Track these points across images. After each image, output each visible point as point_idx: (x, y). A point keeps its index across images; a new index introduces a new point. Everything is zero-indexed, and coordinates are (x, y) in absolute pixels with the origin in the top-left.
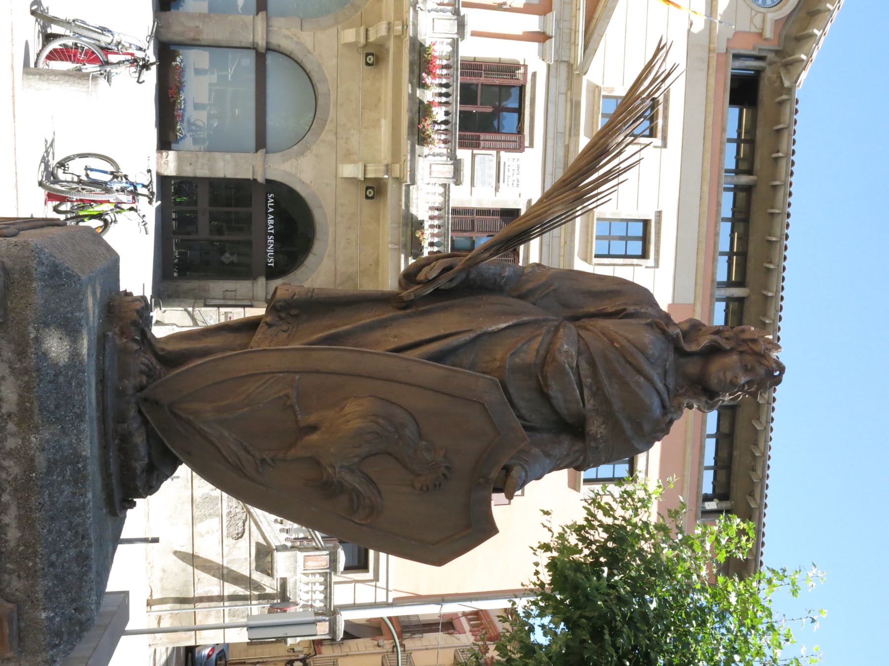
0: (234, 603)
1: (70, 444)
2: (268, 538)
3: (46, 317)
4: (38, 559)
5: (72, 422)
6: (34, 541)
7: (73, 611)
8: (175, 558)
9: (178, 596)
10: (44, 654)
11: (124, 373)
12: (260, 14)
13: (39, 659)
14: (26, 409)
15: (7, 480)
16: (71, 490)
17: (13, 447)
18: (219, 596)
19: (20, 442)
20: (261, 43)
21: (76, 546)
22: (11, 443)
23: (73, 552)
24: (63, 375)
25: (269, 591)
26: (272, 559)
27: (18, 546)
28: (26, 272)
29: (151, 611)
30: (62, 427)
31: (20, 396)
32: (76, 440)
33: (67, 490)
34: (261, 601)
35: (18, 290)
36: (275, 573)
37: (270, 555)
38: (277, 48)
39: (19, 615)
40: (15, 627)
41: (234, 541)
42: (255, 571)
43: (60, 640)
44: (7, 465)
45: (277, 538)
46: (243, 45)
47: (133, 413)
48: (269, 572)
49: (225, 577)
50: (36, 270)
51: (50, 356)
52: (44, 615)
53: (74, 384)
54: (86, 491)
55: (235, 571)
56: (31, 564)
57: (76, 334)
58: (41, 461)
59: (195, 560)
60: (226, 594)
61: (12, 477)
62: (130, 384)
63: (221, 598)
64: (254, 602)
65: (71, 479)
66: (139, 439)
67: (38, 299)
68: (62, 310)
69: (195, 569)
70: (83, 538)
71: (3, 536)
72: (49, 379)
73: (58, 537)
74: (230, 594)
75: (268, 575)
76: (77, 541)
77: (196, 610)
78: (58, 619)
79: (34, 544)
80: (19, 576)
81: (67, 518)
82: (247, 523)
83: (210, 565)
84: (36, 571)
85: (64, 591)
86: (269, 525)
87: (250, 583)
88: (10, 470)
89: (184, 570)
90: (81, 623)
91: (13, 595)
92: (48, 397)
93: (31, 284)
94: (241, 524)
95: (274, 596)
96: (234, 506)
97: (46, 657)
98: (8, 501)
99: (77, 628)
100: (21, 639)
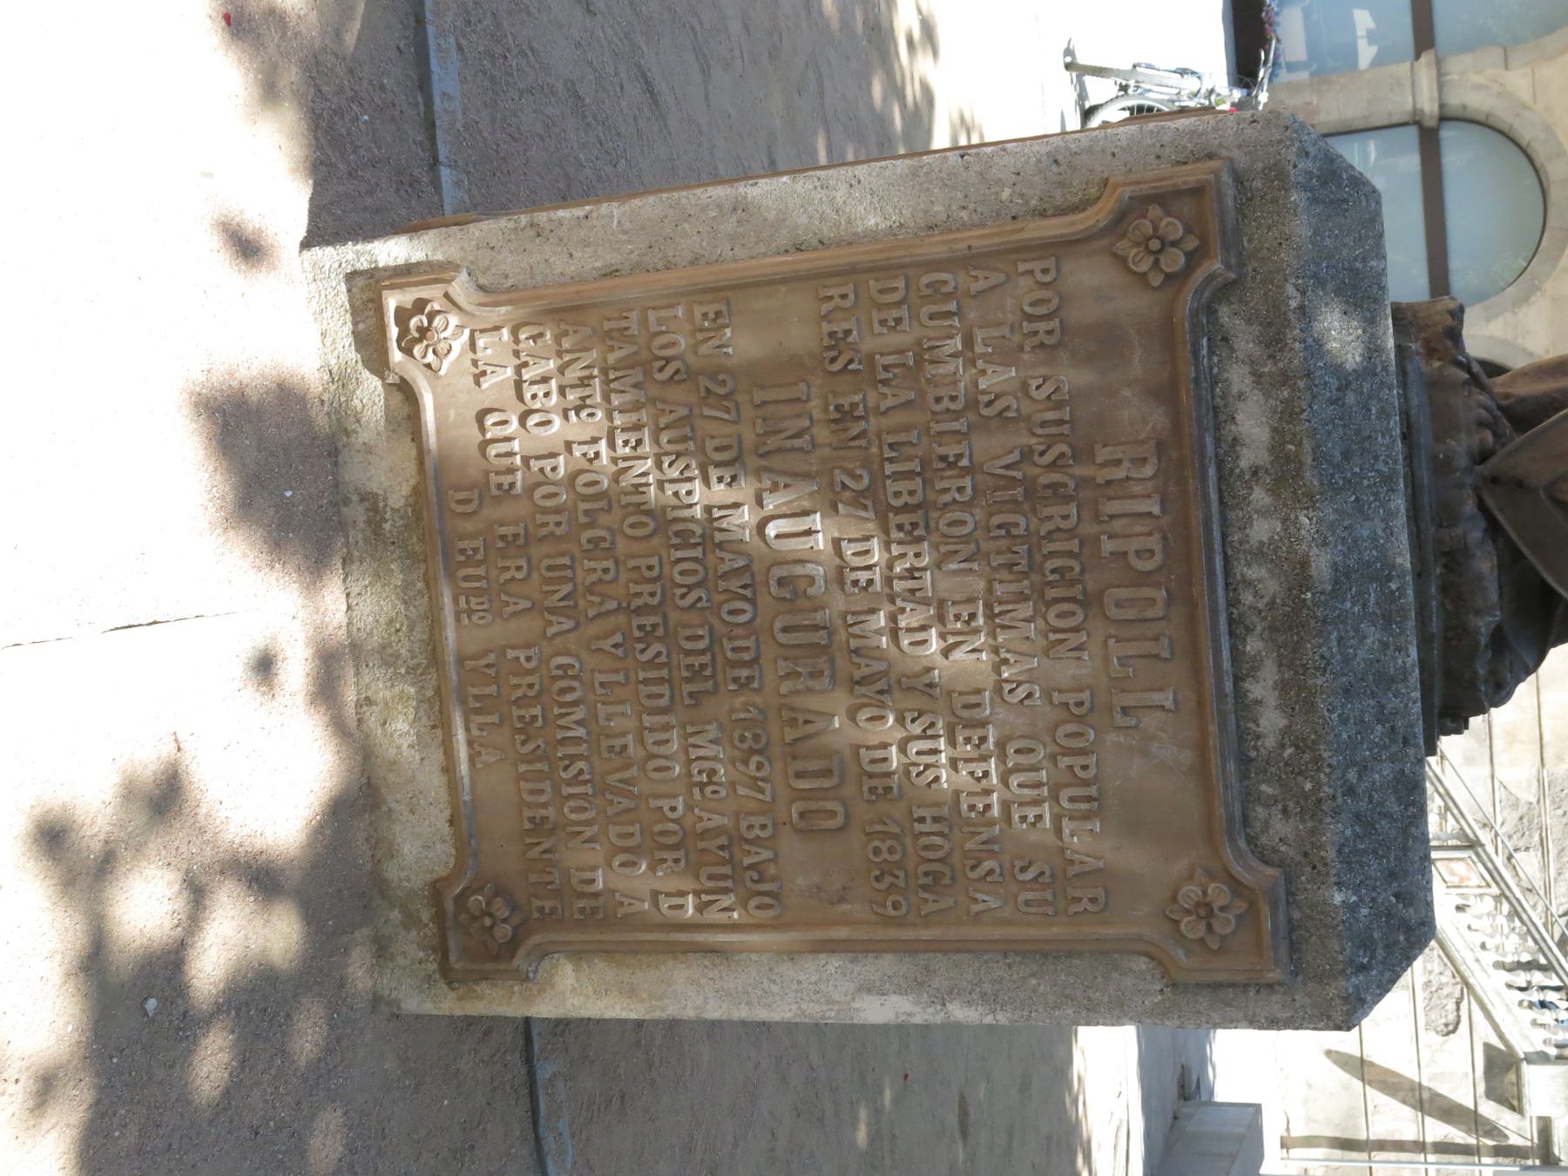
0: (1445, 1158)
1: (1374, 538)
2: (1508, 1036)
3: (1318, 265)
4: (1322, 776)
5: (1374, 490)
6: (1313, 737)
7: (1393, 899)
8: (1328, 1063)
9: (1338, 1135)
10: (1342, 983)
11: (1445, 425)
12: (1424, 59)
13: (1332, 992)
14: (1288, 460)
15: (1255, 608)
16: (1378, 636)
17: (1265, 539)
18: (1416, 1143)
19: (1279, 527)
20: (1429, 107)
21: (1393, 759)
22: (1262, 530)
23: (1387, 770)
24: (1354, 391)
25: (1514, 1140)
26: (1519, 1077)
27: (1283, 746)
28: (1277, 174)
29: (1288, 1159)
30: (1357, 499)
31: (1275, 430)
32: (1384, 530)
33: (1373, 636)
34: (1500, 1159)
35: (1262, 211)
36: (1526, 1107)
37: (1514, 1070)
38: (1460, 114)
39: (1289, 893)
40: (1282, 917)
41: (1442, 1039)
42: (1484, 1099)
43: (1372, 958)
44: (1255, 576)
45: (1526, 1037)
46: (1395, 120)
47: (1470, 507)
48: (1515, 1103)
49: (1426, 1106)
50: (1295, 166)
51: (1328, 346)
52: (1338, 898)
53: (1374, 411)
54: (1406, 641)
55: (1445, 1097)
56: (1308, 786)
57: (1373, 306)
58: (1321, 564)
59: (1366, 1070)
60: (1429, 1139)
61: (1265, 600)
62: (1461, 446)
63: (1419, 1147)
64: (1485, 1160)
65: (1378, 612)
66: (1485, 564)
67: (1301, 228)
68: (1345, 252)
69: (1367, 1087)
70: (1406, 742)
71: (1251, 725)
72: (1328, 395)
73: (1360, 733)
74: (1438, 1140)
75: (1513, 1108)
76: (1393, 749)
77: (1373, 1165)
78: (1364, 911)
79: (1314, 742)
80: (1285, 811)
81: (1373, 695)
82: (1464, 1005)
83: (1396, 1080)
84: (1319, 801)
85: (1375, 852)
86: (1509, 1010)
87: (1476, 1122)
88: (1260, 586)
89: (1347, 1088)
90: (1409, 929)
91: (1275, 851)
92: (1329, 433)
93: (1287, 197)
94: (1451, 1006)
95: (1527, 1152)
96: (1437, 971)
97: (1346, 989)
98: (1259, 651)
99: (1402, 938)
100: (1294, 947)
